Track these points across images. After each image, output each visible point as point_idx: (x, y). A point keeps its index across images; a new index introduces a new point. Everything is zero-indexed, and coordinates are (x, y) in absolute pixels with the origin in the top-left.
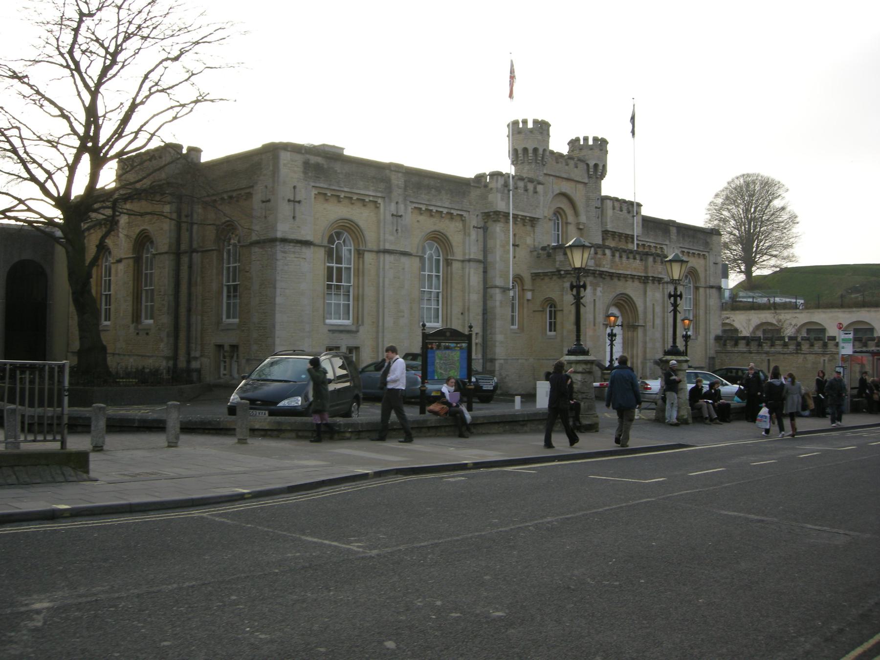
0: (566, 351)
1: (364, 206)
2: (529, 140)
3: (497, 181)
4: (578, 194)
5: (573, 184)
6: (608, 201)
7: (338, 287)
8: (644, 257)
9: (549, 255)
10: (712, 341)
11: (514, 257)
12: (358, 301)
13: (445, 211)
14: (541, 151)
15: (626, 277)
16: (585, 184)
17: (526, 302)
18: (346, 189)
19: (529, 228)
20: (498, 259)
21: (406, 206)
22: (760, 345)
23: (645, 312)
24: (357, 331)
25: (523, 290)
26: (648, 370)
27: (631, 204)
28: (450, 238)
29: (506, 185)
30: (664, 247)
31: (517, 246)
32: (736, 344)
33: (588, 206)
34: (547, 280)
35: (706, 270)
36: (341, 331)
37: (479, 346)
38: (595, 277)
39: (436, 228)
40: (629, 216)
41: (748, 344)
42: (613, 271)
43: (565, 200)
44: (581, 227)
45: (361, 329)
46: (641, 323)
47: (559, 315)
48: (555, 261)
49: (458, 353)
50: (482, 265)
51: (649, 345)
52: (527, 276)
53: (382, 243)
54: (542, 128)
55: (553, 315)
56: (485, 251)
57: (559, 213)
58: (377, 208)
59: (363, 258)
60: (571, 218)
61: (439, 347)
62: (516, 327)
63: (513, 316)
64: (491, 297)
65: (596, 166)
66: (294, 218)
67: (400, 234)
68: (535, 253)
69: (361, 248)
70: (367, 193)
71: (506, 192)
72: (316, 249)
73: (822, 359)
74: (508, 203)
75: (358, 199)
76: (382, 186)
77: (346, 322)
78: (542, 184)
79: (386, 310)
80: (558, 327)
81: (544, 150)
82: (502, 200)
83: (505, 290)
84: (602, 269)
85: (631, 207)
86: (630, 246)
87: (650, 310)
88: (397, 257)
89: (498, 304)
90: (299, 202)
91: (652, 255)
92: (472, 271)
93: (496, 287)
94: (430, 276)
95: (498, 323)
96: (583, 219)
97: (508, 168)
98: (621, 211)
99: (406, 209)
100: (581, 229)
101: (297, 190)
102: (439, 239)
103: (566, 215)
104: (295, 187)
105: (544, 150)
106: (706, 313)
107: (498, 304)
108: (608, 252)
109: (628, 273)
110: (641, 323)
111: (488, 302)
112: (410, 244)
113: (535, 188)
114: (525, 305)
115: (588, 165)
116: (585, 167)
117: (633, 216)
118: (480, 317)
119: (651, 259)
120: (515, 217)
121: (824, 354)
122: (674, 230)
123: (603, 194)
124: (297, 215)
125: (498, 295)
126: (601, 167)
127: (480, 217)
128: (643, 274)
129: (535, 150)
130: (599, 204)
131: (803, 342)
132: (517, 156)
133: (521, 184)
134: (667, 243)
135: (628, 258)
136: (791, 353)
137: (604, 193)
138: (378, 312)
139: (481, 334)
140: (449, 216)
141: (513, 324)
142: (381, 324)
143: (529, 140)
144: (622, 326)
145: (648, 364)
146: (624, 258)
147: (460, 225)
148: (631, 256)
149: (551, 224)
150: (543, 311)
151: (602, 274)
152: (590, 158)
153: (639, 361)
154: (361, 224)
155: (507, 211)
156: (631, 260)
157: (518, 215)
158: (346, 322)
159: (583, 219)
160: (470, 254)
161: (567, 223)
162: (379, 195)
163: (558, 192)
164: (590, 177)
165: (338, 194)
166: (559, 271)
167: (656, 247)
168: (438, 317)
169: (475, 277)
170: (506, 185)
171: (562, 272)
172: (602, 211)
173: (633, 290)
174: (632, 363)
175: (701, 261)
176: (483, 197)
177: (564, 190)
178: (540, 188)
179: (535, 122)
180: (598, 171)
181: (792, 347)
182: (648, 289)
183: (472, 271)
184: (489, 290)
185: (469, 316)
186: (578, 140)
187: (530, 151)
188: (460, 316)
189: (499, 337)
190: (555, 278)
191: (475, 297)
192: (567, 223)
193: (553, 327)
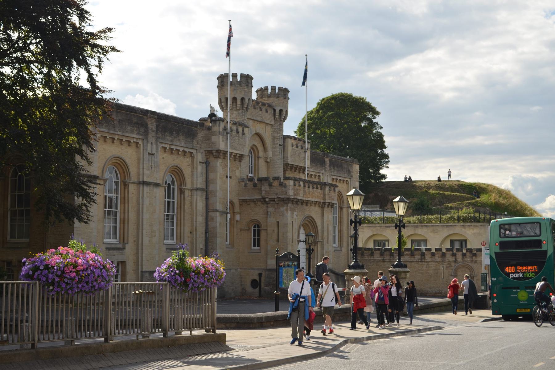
3: (219, 126)
4: (267, 134)
5: (263, 125)
9: (255, 185)
12: (124, 223)
17: (235, 223)
18: (119, 133)
20: (218, 189)
21: (157, 145)
23: (323, 231)
24: (124, 248)
28: (184, 171)
30: (321, 175)
33: (273, 143)
38: (293, 203)
42: (305, 199)
43: (258, 139)
44: (268, 160)
47: (263, 234)
48: (260, 190)
53: (141, 177)
55: (257, 233)
56: (207, 181)
60: (261, 154)
61: (284, 266)
64: (213, 219)
67: (153, 168)
68: (243, 183)
71: (225, 134)
73: (441, 266)
74: (227, 143)
76: (142, 130)
77: (114, 241)
78: (248, 127)
79: (144, 231)
80: (262, 242)
81: (249, 99)
86: (302, 176)
87: (326, 229)
88: (151, 187)
92: (199, 198)
93: (217, 211)
95: (219, 240)
98: (297, 147)
99: (157, 149)
102: (177, 172)
105: (249, 99)
107: (218, 225)
109: (313, 200)
110: (320, 239)
111: (210, 223)
112: (157, 178)
113: (243, 131)
114: (235, 226)
115: (274, 110)
117: (227, 133)
121: (443, 262)
122: (152, 125)
125: (218, 218)
126: (284, 113)
127: (204, 154)
130: (281, 142)
131: (426, 253)
133: (234, 128)
134: (324, 172)
135: (313, 188)
136: (417, 262)
142: (140, 242)
143: (233, 86)
144: (305, 241)
147: (189, 160)
148: (315, 186)
150: (249, 229)
155: (225, 150)
156: (315, 190)
158: (114, 241)
159: (270, 154)
160: (197, 185)
161: (258, 157)
164: (275, 119)
166: (264, 199)
167: (315, 175)
168: (172, 235)
169: (200, 205)
171: (267, 200)
172: (284, 149)
173: (314, 212)
174: (280, 35)
176: (208, 139)
177: (258, 131)
178: (246, 130)
181: (417, 257)
183: (199, 198)
185: (196, 234)
186: (266, 88)
188: (189, 235)
191: (201, 219)
193: (257, 243)
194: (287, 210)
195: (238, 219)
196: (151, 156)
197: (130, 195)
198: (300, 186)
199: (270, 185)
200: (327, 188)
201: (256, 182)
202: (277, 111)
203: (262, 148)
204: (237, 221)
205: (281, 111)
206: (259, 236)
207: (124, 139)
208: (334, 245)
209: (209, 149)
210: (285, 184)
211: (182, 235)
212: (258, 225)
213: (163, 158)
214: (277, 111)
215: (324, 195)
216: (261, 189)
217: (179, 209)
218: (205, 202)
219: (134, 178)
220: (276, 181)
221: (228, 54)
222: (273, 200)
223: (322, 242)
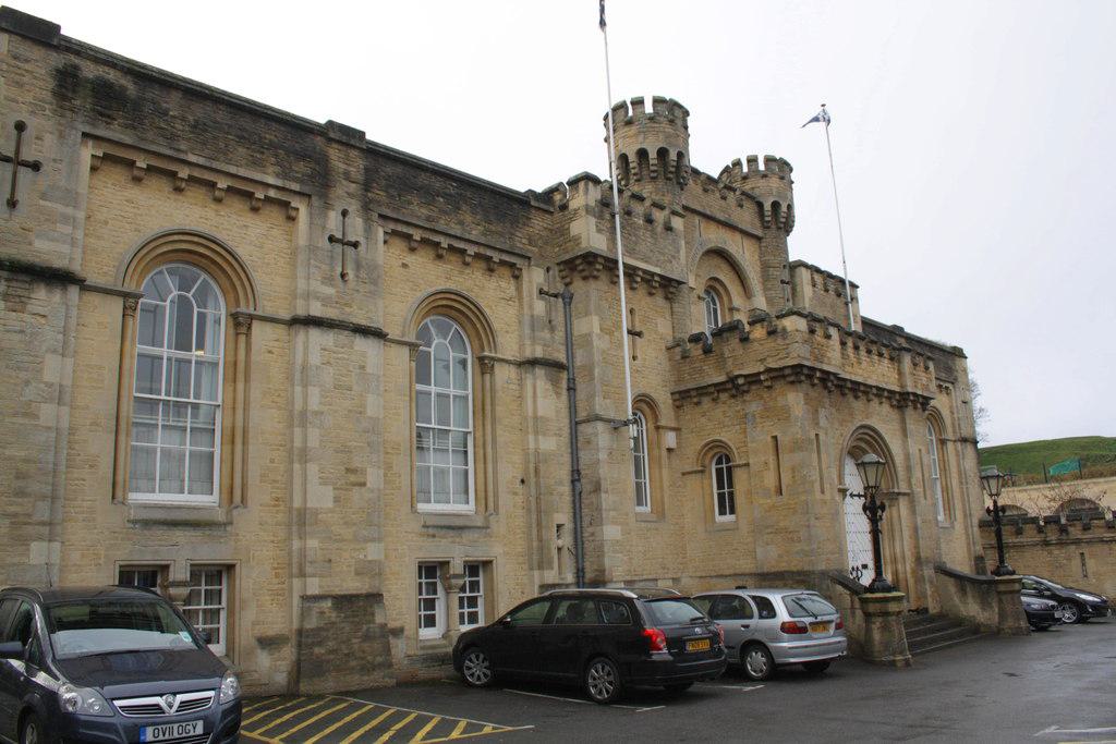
2: (652, 140)
4: (746, 254)
6: (803, 270)
7: (32, 334)
8: (895, 354)
9: (707, 351)
10: (976, 529)
11: (634, 358)
14: (673, 156)
16: (759, 239)
17: (664, 453)
18: (192, 158)
19: (659, 300)
21: (367, 220)
22: (1063, 530)
23: (909, 469)
25: (658, 428)
28: (487, 311)
29: (605, 203)
31: (639, 334)
34: (706, 402)
35: (952, 413)
37: (565, 552)
40: (839, 302)
46: (903, 488)
47: (740, 476)
48: (722, 359)
52: (663, 399)
54: (672, 114)
55: (725, 478)
58: (292, 219)
59: (248, 335)
62: (647, 509)
63: (638, 486)
69: (243, 309)
70: (258, 176)
71: (608, 216)
74: (613, 240)
75: (191, 179)
76: (301, 168)
80: (740, 501)
83: (617, 426)
84: (826, 368)
85: (839, 288)
89: (603, 456)
90: (36, 166)
93: (598, 418)
95: (607, 500)
98: (827, 291)
99: (368, 230)
101: (25, 135)
104: (20, 127)
111: (581, 454)
115: (760, 205)
120: (631, 272)
123: (792, 258)
124: (19, 196)
125: (601, 435)
126: (784, 208)
129: (642, 154)
137: (794, 255)
139: (569, 527)
140: (483, 265)
141: (639, 503)
143: (652, 140)
146: (863, 352)
148: (874, 349)
149: (703, 305)
154: (242, 251)
157: (635, 269)
162: (295, 187)
164: (765, 226)
170: (605, 203)
171: (741, 381)
172: (794, 290)
174: (896, 574)
180: (779, 219)
184: (581, 428)
186: (737, 163)
187: (653, 155)
189: (611, 532)
190: (724, 396)
193: (727, 504)
195: (673, 444)
196: (338, 248)
197: (254, 357)
198: (828, 337)
199: (745, 339)
200: (907, 359)
201: (710, 341)
202: (767, 207)
203: (740, 289)
205: (776, 205)
206: (731, 485)
207: (223, 183)
208: (639, 509)
209: (567, 257)
210: (784, 329)
211: (490, 487)
212: (727, 456)
213: (405, 266)
214: (767, 207)
216: (722, 354)
217: (479, 416)
220: (758, 325)
221: (602, 23)
222: (753, 379)
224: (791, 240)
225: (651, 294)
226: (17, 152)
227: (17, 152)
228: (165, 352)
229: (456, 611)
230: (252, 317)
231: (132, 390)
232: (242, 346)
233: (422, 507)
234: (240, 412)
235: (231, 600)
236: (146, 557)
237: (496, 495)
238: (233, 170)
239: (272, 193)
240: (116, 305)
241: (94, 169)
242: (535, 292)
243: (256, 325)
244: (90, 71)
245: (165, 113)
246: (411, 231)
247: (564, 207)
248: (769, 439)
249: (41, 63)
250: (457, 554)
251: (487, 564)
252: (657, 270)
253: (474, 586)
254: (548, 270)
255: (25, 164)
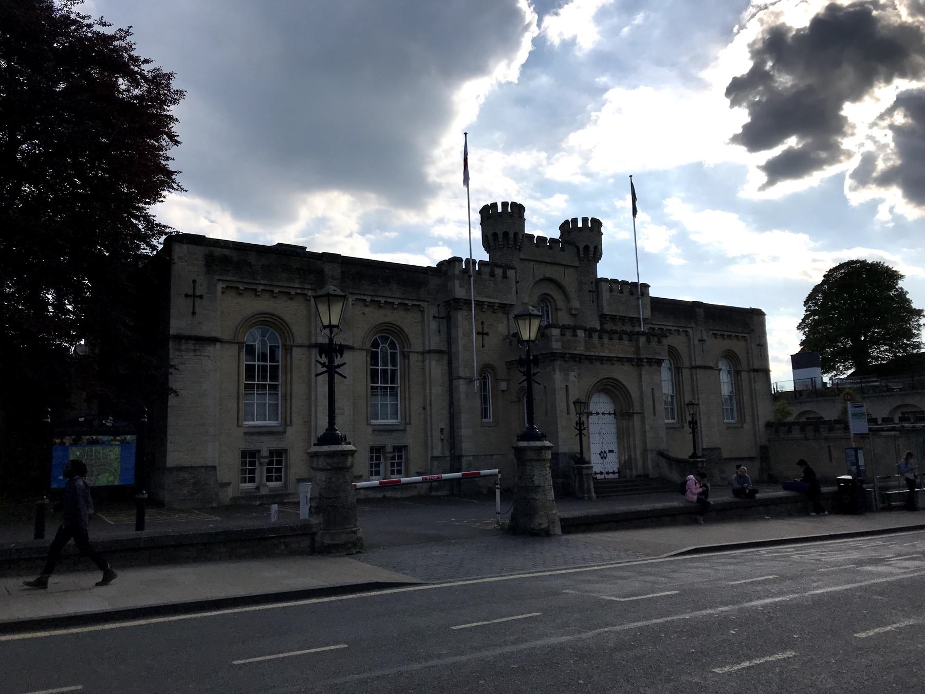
0: (314, 440)
1: (291, 299)
2: (501, 222)
4: (569, 279)
6: (603, 283)
13: (397, 302)
15: (609, 359)
18: (262, 282)
19: (500, 315)
23: (642, 399)
26: (649, 463)
27: (634, 284)
30: (689, 330)
32: (789, 431)
36: (259, 434)
39: (387, 320)
41: (803, 430)
44: (573, 312)
45: (289, 430)
49: (117, 450)
50: (446, 357)
51: (649, 434)
57: (545, 299)
59: (291, 353)
60: (561, 304)
65: (586, 248)
66: (194, 313)
69: (288, 343)
70: (292, 285)
71: (466, 277)
72: (226, 346)
77: (671, 421)
81: (516, 234)
82: (461, 286)
83: (470, 381)
91: (656, 335)
92: (433, 363)
93: (460, 378)
94: (385, 372)
96: (576, 304)
97: (482, 255)
100: (575, 315)
103: (555, 301)
104: (194, 281)
105: (516, 234)
106: (752, 399)
108: (580, 333)
110: (637, 409)
113: (505, 273)
115: (578, 248)
116: (575, 250)
117: (638, 298)
118: (445, 412)
119: (642, 339)
120: (479, 304)
125: (462, 386)
128: (633, 356)
129: (506, 234)
132: (488, 243)
138: (310, 410)
141: (486, 417)
144: (615, 414)
145: (649, 456)
146: (606, 341)
151: (578, 359)
152: (582, 238)
153: (638, 452)
154: (287, 318)
158: (671, 421)
159: (576, 304)
161: (556, 310)
163: (542, 277)
164: (580, 260)
165: (255, 287)
172: (598, 298)
175: (742, 343)
177: (548, 276)
178: (511, 273)
179: (585, 220)
180: (596, 253)
182: (643, 372)
186: (494, 205)
187: (500, 236)
192: (556, 310)
194: (554, 370)
202: (581, 249)
204: (503, 391)
207: (276, 290)
213: (364, 314)
214: (581, 249)
215: (638, 348)
218: (446, 368)
219: (687, 364)
223: (641, 413)
224: (600, 266)
225: (494, 312)
226: (194, 292)
227: (194, 292)
228: (268, 363)
229: (389, 468)
230: (292, 346)
231: (244, 381)
232: (289, 358)
233: (374, 422)
234: (289, 386)
235: (286, 462)
236: (252, 447)
237: (410, 416)
238: (280, 284)
239: (299, 291)
240: (236, 347)
241: (223, 293)
242: (431, 318)
243: (294, 349)
244: (218, 251)
245: (250, 264)
246: (406, 302)
247: (445, 274)
248: (361, 473)
249: (200, 251)
250: (389, 442)
251: (405, 447)
252: (497, 301)
253: (400, 457)
254: (438, 306)
255: (190, 296)
